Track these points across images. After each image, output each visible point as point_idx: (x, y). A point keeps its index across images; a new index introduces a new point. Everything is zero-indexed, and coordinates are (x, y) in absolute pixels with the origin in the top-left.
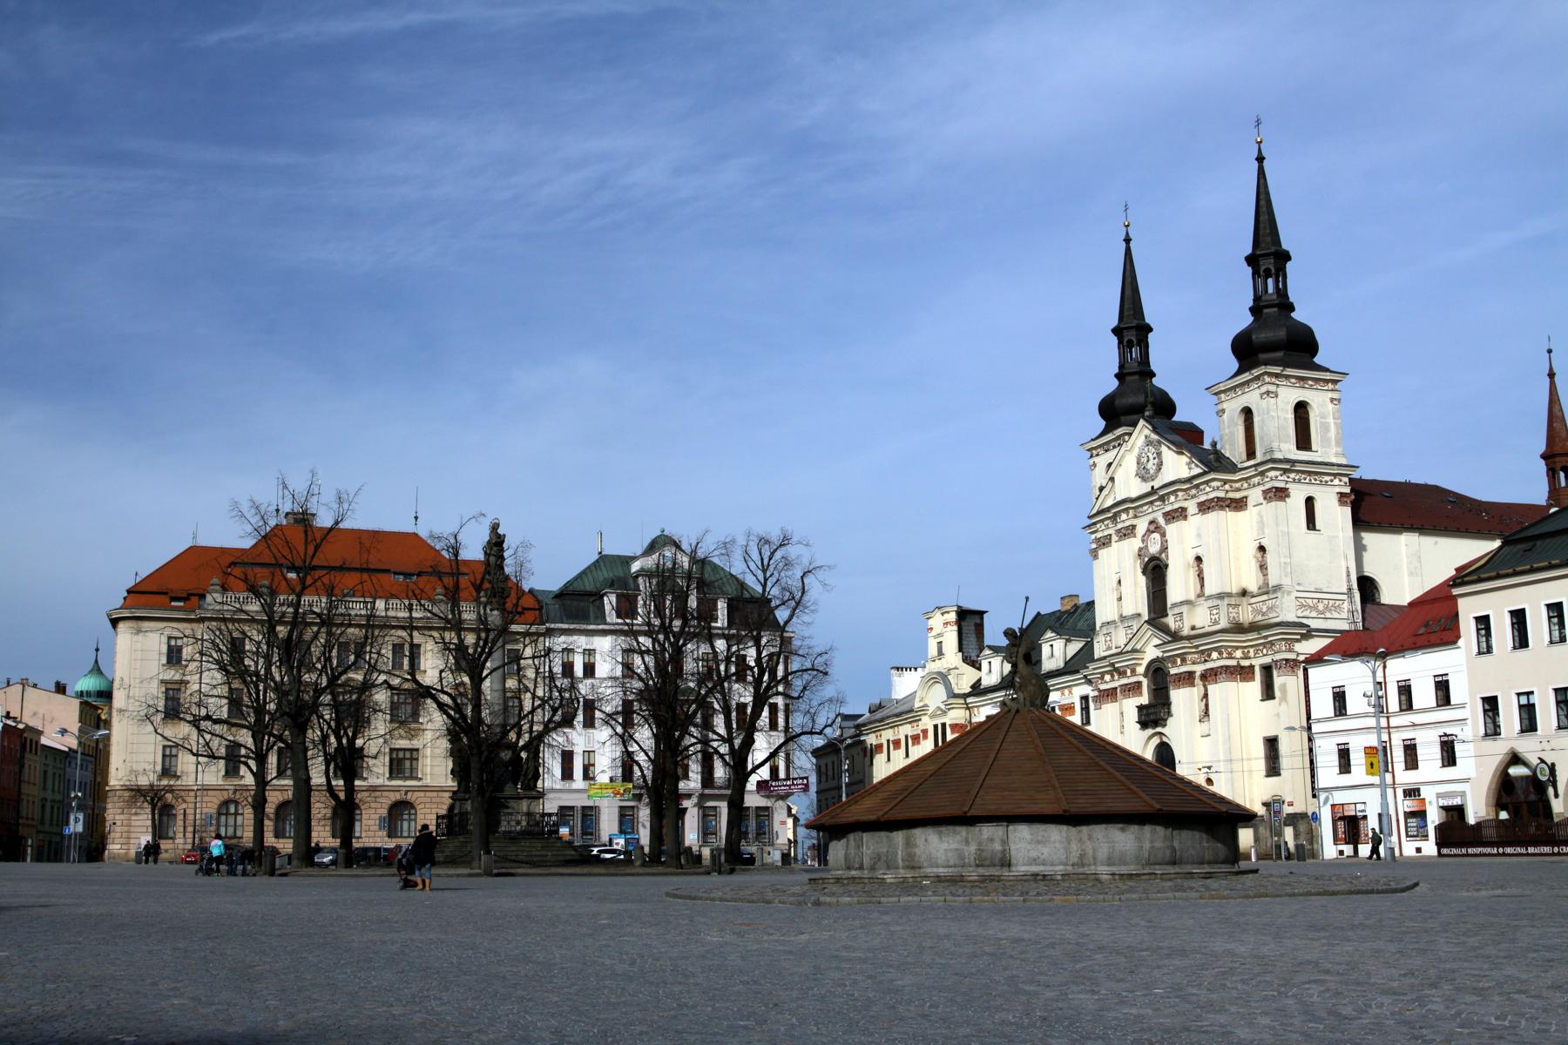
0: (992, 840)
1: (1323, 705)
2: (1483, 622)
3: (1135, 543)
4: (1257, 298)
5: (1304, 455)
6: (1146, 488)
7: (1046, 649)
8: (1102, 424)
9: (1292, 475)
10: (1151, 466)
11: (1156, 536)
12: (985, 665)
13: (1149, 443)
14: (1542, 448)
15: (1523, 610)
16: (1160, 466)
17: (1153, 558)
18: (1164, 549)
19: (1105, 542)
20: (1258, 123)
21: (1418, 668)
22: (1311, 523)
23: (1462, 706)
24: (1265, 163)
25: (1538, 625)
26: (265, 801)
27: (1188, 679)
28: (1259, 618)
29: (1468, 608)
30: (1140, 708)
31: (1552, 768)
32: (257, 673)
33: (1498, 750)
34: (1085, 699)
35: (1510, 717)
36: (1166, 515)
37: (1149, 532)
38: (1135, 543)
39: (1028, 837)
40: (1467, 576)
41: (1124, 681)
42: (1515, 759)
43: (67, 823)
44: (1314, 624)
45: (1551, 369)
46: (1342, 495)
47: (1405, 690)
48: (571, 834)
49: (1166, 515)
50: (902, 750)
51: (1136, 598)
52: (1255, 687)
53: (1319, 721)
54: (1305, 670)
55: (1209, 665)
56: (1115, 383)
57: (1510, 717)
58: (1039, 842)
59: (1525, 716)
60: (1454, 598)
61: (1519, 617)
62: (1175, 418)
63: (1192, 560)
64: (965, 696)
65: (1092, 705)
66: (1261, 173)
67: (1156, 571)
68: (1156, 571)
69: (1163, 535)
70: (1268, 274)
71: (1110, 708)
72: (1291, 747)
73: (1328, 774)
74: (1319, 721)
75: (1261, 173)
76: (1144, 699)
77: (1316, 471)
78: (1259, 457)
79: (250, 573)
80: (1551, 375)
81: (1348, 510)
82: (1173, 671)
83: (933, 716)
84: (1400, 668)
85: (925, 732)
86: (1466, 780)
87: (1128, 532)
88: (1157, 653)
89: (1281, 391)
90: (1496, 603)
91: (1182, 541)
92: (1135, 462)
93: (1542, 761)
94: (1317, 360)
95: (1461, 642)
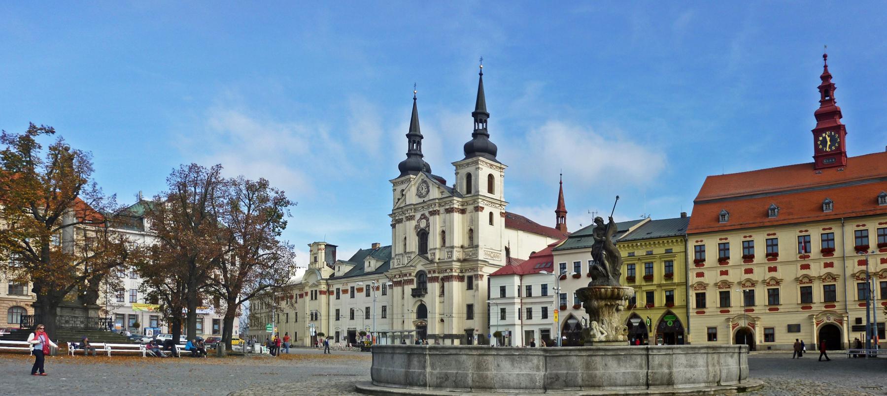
0: (661, 365)
1: (496, 293)
2: (563, 266)
3: (414, 223)
4: (475, 130)
6: (421, 200)
7: (366, 264)
8: (399, 173)
10: (424, 192)
11: (424, 221)
12: (337, 268)
13: (424, 182)
14: (556, 209)
16: (428, 192)
17: (422, 230)
18: (428, 226)
19: (400, 221)
21: (535, 283)
22: (491, 222)
23: (552, 296)
26: (534, 256)
27: (434, 279)
29: (557, 261)
30: (413, 290)
34: (368, 286)
36: (430, 212)
37: (421, 219)
38: (414, 223)
39: (685, 362)
41: (406, 278)
42: (571, 317)
43: (97, 296)
44: (491, 262)
45: (826, 77)
47: (529, 288)
49: (430, 212)
51: (413, 244)
52: (465, 284)
54: (489, 280)
55: (446, 274)
58: (691, 366)
60: (552, 256)
64: (327, 280)
67: (423, 235)
68: (423, 235)
69: (428, 220)
70: (414, 142)
71: (397, 290)
72: (477, 310)
73: (495, 319)
76: (415, 286)
77: (492, 202)
78: (473, 192)
80: (561, 183)
82: (429, 276)
83: (310, 287)
84: (528, 281)
85: (307, 294)
86: (551, 324)
87: (411, 218)
88: (422, 268)
91: (436, 224)
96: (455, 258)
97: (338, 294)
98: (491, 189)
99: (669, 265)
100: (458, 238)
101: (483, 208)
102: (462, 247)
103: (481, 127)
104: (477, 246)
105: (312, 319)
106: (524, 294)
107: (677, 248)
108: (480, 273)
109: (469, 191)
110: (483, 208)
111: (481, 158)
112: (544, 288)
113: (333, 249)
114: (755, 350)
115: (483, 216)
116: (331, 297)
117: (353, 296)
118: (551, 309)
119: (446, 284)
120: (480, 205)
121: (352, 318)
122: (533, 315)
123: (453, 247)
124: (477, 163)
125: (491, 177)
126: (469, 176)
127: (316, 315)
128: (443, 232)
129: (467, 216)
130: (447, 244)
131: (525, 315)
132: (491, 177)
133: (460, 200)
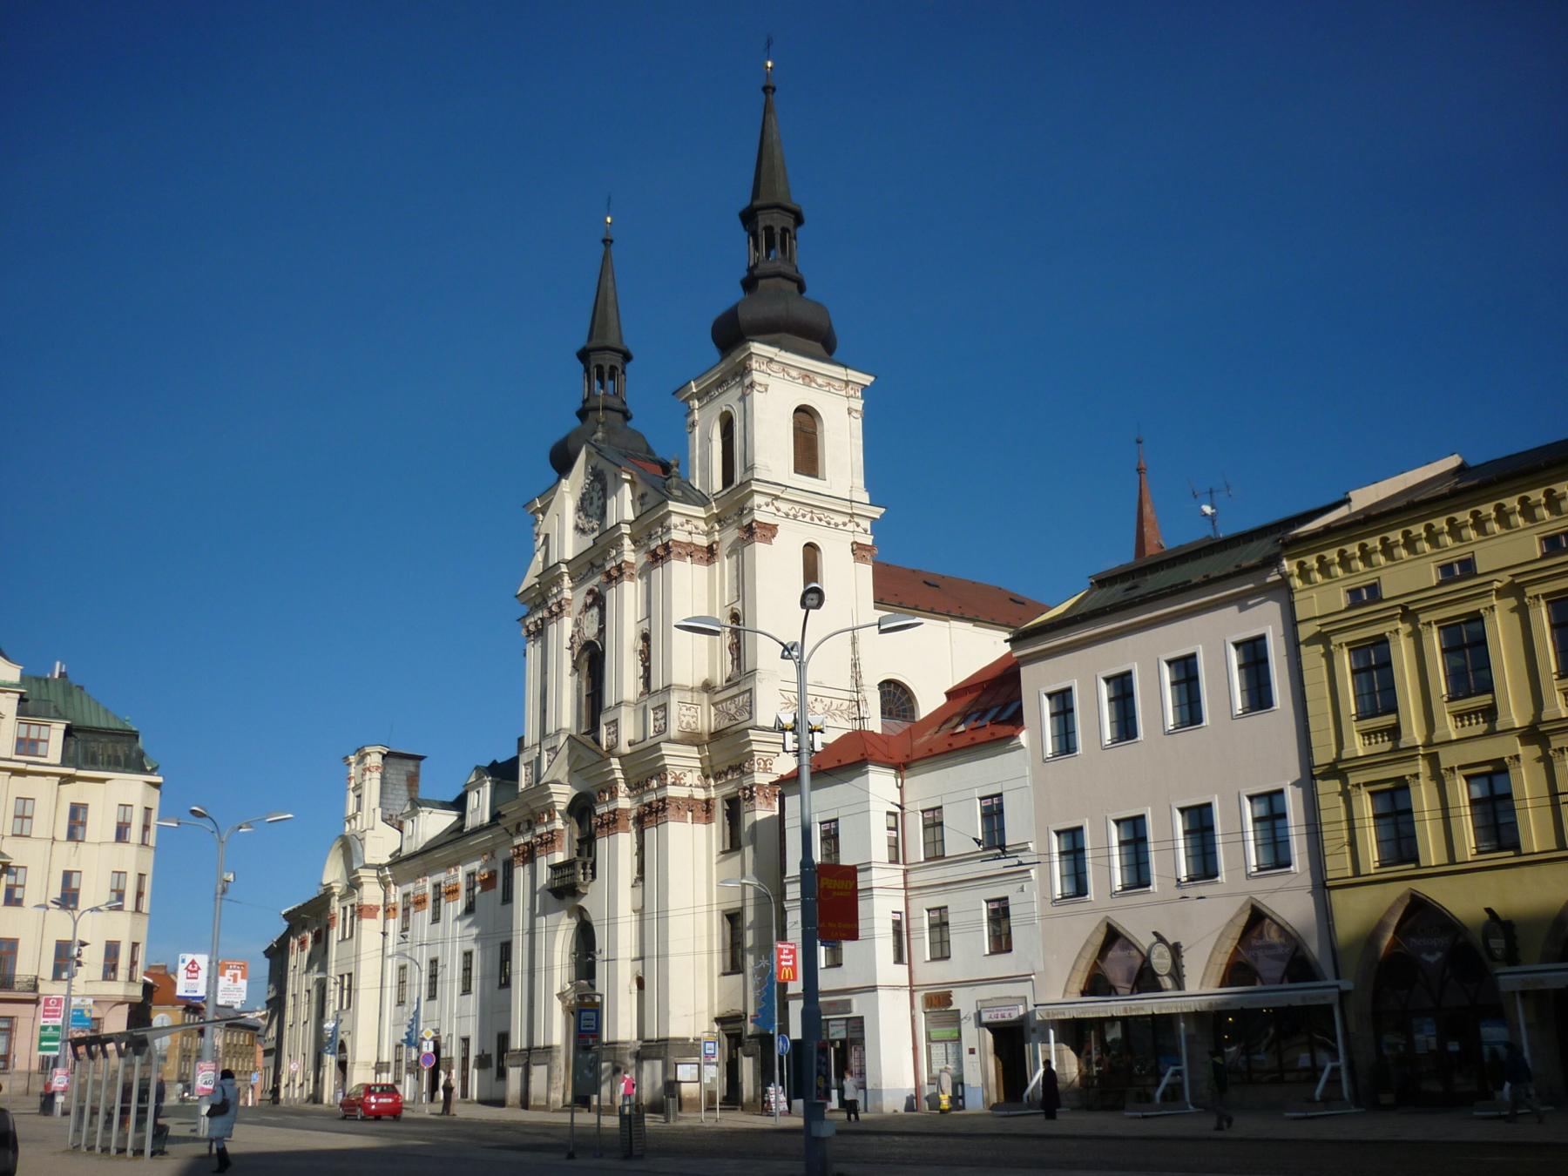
2: (1062, 702)
9: (784, 507)
15: (1192, 657)
18: (602, 631)
20: (769, 43)
21: (959, 788)
28: (726, 723)
29: (1037, 684)
31: (1176, 950)
33: (1083, 927)
35: (1108, 864)
45: (91, 910)
47: (934, 823)
48: (832, 1111)
50: (427, 913)
59: (728, 926)
61: (1186, 671)
64: (380, 868)
68: (592, 659)
77: (815, 509)
78: (738, 479)
81: (866, 571)
84: (926, 787)
86: (1024, 978)
89: (543, 530)
90: (1083, 674)
93: (1161, 939)
94: (834, 356)
95: (1023, 737)
96: (674, 731)
101: (770, 530)
102: (707, 687)
106: (916, 849)
109: (728, 478)
110: (770, 530)
112: (993, 813)
113: (410, 766)
114: (771, 1115)
115: (776, 568)
118: (1027, 904)
119: (651, 833)
120: (759, 516)
122: (956, 940)
123: (667, 689)
124: (743, 371)
125: (806, 421)
128: (646, 638)
129: (724, 565)
130: (657, 684)
131: (922, 945)
132: (806, 421)
133: (699, 512)
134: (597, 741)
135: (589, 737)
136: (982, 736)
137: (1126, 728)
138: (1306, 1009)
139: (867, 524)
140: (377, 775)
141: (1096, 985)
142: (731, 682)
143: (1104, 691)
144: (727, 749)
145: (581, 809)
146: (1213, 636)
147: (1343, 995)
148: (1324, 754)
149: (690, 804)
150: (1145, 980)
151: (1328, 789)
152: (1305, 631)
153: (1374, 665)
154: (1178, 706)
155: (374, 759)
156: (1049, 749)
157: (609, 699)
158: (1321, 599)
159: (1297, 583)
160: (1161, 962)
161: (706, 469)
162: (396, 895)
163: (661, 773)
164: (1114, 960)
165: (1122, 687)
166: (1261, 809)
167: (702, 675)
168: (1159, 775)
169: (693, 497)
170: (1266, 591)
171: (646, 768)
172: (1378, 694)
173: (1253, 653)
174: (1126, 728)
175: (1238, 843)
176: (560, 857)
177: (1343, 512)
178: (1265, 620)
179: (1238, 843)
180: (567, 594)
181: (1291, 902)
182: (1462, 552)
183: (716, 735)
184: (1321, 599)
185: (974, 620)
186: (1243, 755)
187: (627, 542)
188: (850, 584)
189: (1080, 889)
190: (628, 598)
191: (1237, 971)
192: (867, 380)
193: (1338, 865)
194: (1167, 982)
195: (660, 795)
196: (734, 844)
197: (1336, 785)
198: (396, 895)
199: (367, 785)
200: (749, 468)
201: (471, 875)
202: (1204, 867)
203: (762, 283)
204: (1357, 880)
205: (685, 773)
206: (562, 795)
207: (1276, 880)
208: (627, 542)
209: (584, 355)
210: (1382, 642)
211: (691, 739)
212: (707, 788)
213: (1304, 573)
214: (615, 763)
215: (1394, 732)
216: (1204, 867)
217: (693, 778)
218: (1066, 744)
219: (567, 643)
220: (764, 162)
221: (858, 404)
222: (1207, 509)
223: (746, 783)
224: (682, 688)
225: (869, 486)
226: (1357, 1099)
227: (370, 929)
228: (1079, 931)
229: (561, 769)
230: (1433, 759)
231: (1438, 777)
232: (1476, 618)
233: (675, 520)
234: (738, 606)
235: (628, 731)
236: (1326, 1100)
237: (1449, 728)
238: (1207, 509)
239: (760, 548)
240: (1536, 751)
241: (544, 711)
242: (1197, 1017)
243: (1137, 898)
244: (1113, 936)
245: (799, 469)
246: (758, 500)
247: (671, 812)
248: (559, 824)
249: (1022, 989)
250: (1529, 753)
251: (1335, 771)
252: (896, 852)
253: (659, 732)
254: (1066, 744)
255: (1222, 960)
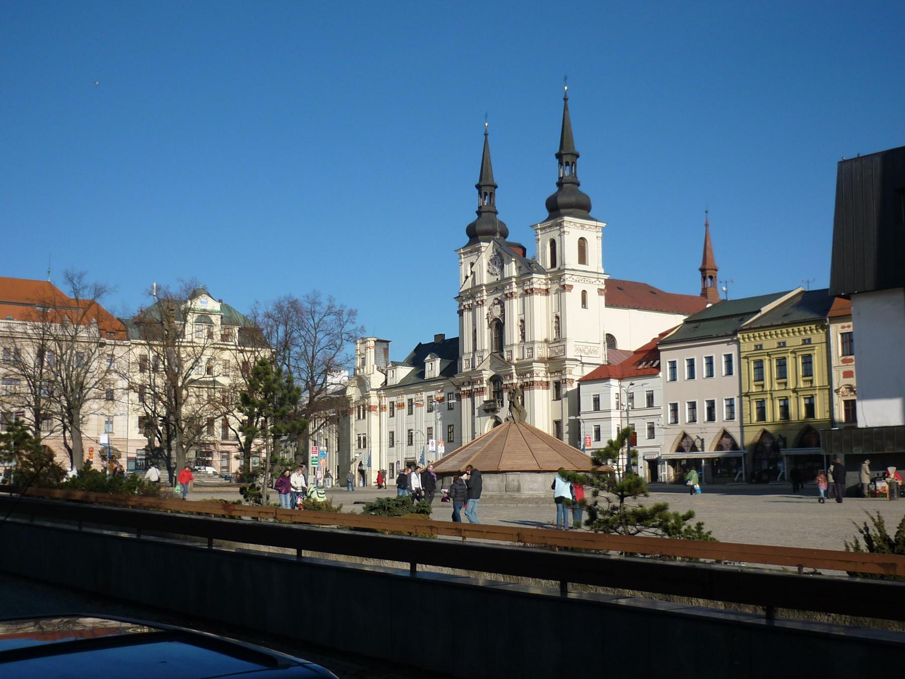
2: (673, 365)
5: (582, 267)
8: (468, 239)
9: (575, 277)
12: (390, 373)
20: (566, 78)
21: (641, 387)
24: (568, 102)
25: (701, 368)
28: (554, 355)
29: (666, 357)
31: (702, 440)
32: (34, 377)
33: (677, 432)
35: (684, 413)
40: (664, 341)
46: (601, 290)
50: (405, 410)
53: (585, 413)
56: (476, 216)
57: (684, 413)
60: (659, 351)
62: (507, 240)
63: (603, 339)
64: (378, 390)
65: (395, 409)
66: (486, 142)
67: (498, 326)
68: (498, 326)
69: (503, 307)
74: (585, 413)
75: (486, 142)
78: (558, 265)
79: (319, 371)
90: (680, 356)
92: (481, 265)
94: (591, 214)
95: (660, 374)
96: (536, 358)
97: (392, 409)
98: (582, 259)
99: (808, 361)
100: (541, 330)
101: (571, 287)
102: (546, 341)
103: (567, 173)
104: (565, 339)
105: (359, 447)
107: (818, 337)
108: (568, 376)
109: (554, 264)
110: (571, 287)
111: (566, 218)
112: (650, 398)
113: (385, 345)
115: (572, 298)
116: (383, 413)
117: (410, 413)
120: (567, 283)
121: (410, 443)
123: (533, 342)
124: (560, 225)
125: (582, 242)
126: (553, 243)
127: (364, 439)
129: (553, 297)
130: (528, 339)
132: (582, 242)
133: (543, 276)
134: (503, 357)
135: (497, 354)
136: (648, 372)
137: (692, 375)
138: (695, 459)
139: (603, 281)
140: (373, 350)
141: (680, 449)
142: (556, 341)
143: (686, 363)
144: (556, 364)
145: (495, 380)
146: (719, 351)
147: (745, 454)
148: (745, 390)
149: (541, 383)
150: (694, 448)
151: (745, 399)
152: (743, 355)
153: (759, 366)
154: (707, 371)
155: (371, 343)
156: (668, 379)
157: (507, 341)
158: (748, 346)
159: (741, 341)
160: (698, 444)
161: (544, 258)
162: (386, 402)
163: (532, 372)
164: (685, 443)
165: (691, 363)
166: (728, 403)
167: (544, 337)
168: (701, 390)
169: (542, 271)
170: (733, 341)
171: (525, 369)
172: (760, 377)
173: (729, 358)
174: (692, 375)
175: (721, 412)
176: (486, 398)
177: (759, 315)
178: (732, 349)
179: (721, 412)
180: (485, 298)
181: (734, 429)
182: (783, 340)
183: (550, 359)
184: (748, 346)
185: (638, 308)
186: (723, 388)
187: (514, 284)
188: (597, 301)
189: (676, 422)
190: (515, 307)
191: (719, 447)
192: (604, 225)
193: (746, 420)
194: (700, 449)
195: (531, 380)
196: (558, 397)
197: (747, 398)
198: (386, 402)
199: (368, 355)
200: (563, 264)
201: (430, 397)
202: (711, 417)
203: (565, 185)
204: (751, 425)
205: (540, 372)
206: (487, 374)
207: (730, 423)
208: (514, 284)
209: (478, 187)
210: (761, 361)
211: (541, 360)
212: (547, 377)
213: (744, 339)
214: (513, 367)
215: (763, 386)
216: (711, 417)
217: (542, 374)
218: (674, 378)
219: (486, 317)
220: (565, 141)
221: (600, 234)
222: (724, 289)
223: (563, 377)
224: (538, 342)
225: (604, 266)
226: (746, 481)
227: (374, 418)
228: (675, 433)
229: (487, 365)
230: (771, 394)
231: (772, 399)
232: (784, 358)
233: (535, 280)
234: (559, 314)
235: (516, 355)
236: (738, 481)
237: (776, 387)
238: (724, 289)
239: (567, 293)
240: (795, 395)
241: (475, 340)
242: (707, 459)
243: (693, 425)
244: (685, 436)
245: (580, 263)
246: (567, 276)
247: (535, 386)
248: (485, 385)
249: (658, 450)
250: (793, 395)
251: (747, 395)
252: (619, 405)
253: (530, 357)
254: (674, 378)
255: (715, 444)
